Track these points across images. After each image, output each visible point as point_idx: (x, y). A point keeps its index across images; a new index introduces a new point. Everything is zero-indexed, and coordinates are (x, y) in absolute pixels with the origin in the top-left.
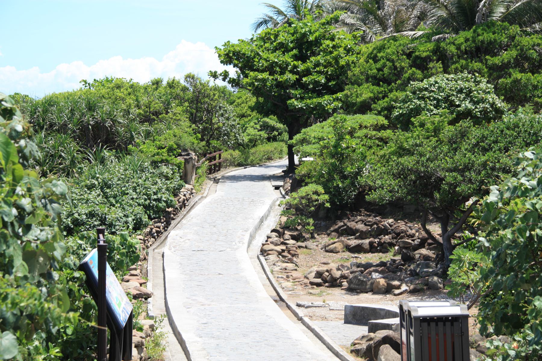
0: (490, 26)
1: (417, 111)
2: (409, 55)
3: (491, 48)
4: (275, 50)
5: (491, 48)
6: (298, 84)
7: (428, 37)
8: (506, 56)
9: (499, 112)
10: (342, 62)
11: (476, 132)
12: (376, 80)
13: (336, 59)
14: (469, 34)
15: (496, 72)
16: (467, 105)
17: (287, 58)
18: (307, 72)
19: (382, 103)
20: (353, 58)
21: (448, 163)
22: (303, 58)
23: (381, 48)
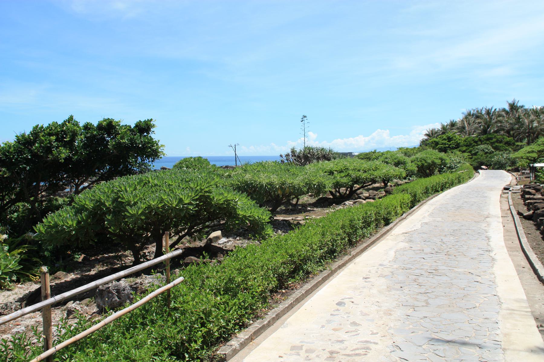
0: (490, 134)
1: (477, 152)
3: (491, 139)
5: (491, 139)
6: (449, 147)
7: (477, 136)
8: (494, 140)
9: (493, 152)
11: (489, 156)
12: (466, 146)
14: (486, 136)
15: (492, 144)
16: (487, 151)
19: (468, 150)
22: (449, 141)
23: (467, 139)
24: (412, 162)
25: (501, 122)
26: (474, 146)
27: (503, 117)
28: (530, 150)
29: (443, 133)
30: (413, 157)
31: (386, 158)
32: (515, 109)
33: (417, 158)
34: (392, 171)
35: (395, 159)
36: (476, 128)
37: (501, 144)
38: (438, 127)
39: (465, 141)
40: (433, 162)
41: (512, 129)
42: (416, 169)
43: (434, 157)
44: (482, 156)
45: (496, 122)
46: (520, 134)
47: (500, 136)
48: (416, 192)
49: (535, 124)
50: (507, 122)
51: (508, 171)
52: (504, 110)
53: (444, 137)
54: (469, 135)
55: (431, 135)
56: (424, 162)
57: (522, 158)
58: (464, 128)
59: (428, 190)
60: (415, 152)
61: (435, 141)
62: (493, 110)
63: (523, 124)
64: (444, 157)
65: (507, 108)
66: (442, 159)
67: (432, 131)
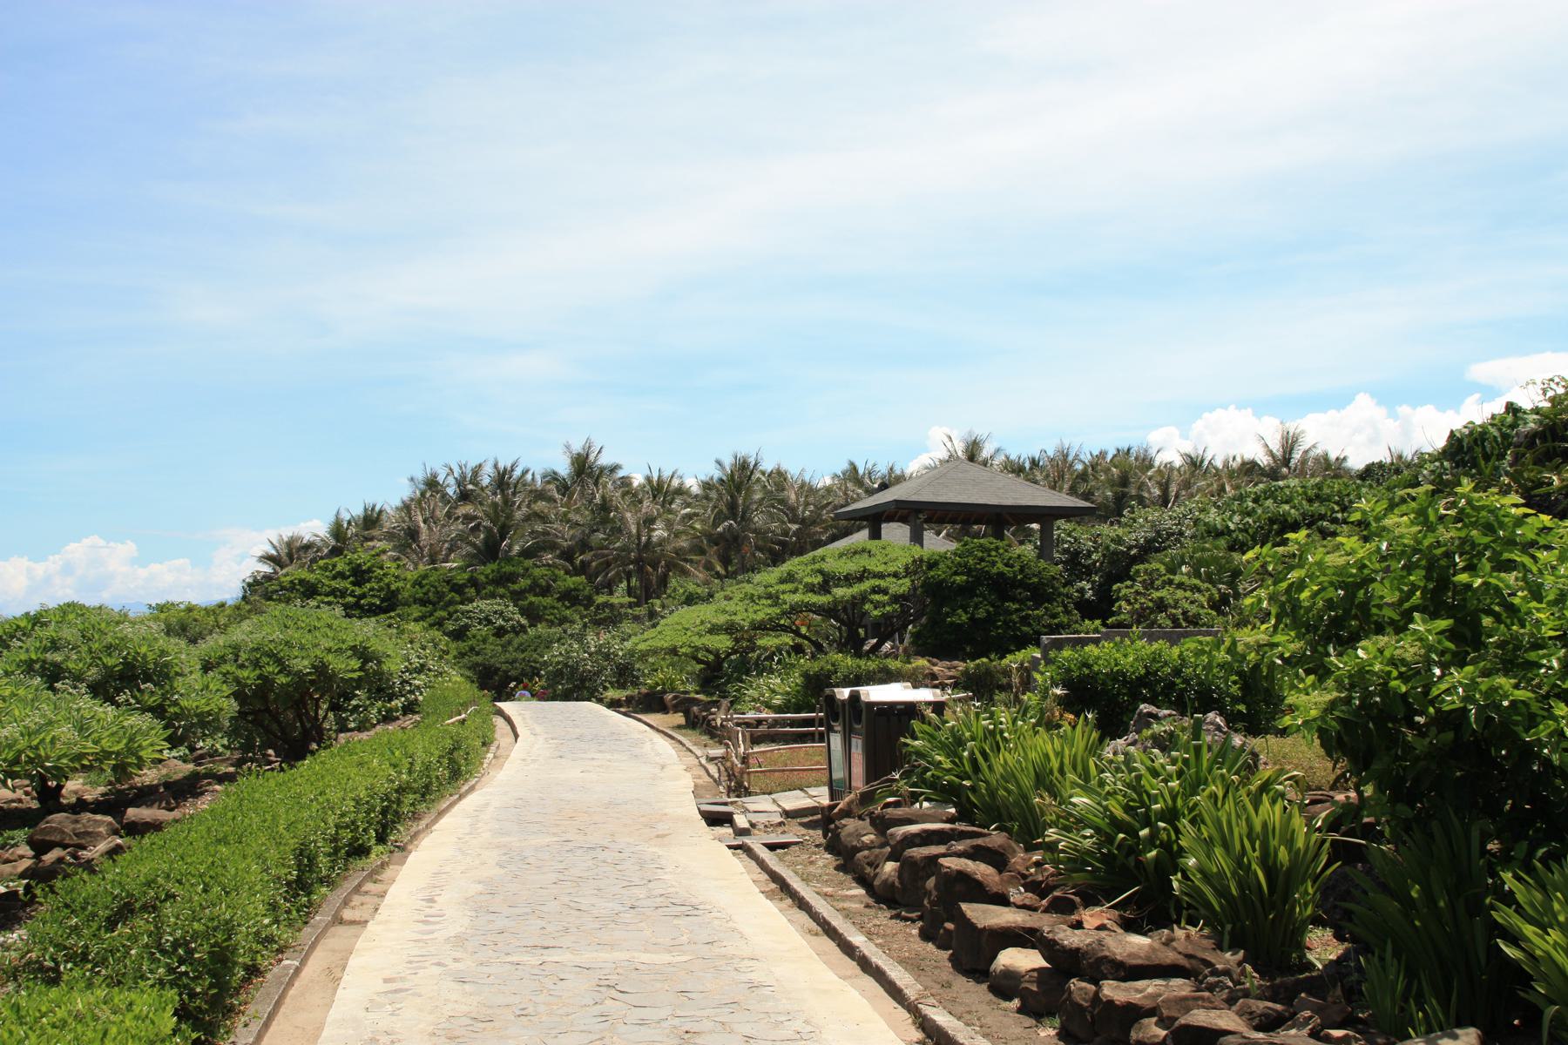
0: (509, 560)
1: (466, 627)
2: (448, 582)
4: (334, 578)
7: (462, 569)
8: (524, 583)
10: (393, 587)
13: (388, 585)
14: (494, 566)
15: (517, 596)
16: (501, 622)
17: (346, 584)
18: (363, 596)
20: (400, 584)
21: (503, 658)
23: (425, 576)
24: (207, 667)
25: (542, 518)
26: (451, 603)
27: (551, 500)
28: (722, 619)
29: (336, 552)
30: (214, 644)
31: (55, 646)
32: (590, 475)
33: (236, 649)
34: (65, 731)
35: (109, 649)
36: (462, 537)
37: (547, 601)
38: (315, 528)
39: (418, 583)
40: (321, 669)
41: (584, 545)
42: (231, 707)
43: (326, 643)
44: (484, 641)
45: (527, 518)
46: (608, 564)
47: (544, 571)
48: (229, 928)
49: (659, 532)
50: (565, 519)
51: (614, 705)
52: (552, 477)
53: (339, 568)
54: (433, 562)
55: (285, 558)
56: (271, 668)
57: (673, 651)
58: (413, 534)
59: (312, 860)
60: (222, 621)
61: (302, 582)
62: (517, 473)
63: (618, 531)
64: (375, 645)
65: (564, 468)
66: (363, 654)
67: (289, 544)
